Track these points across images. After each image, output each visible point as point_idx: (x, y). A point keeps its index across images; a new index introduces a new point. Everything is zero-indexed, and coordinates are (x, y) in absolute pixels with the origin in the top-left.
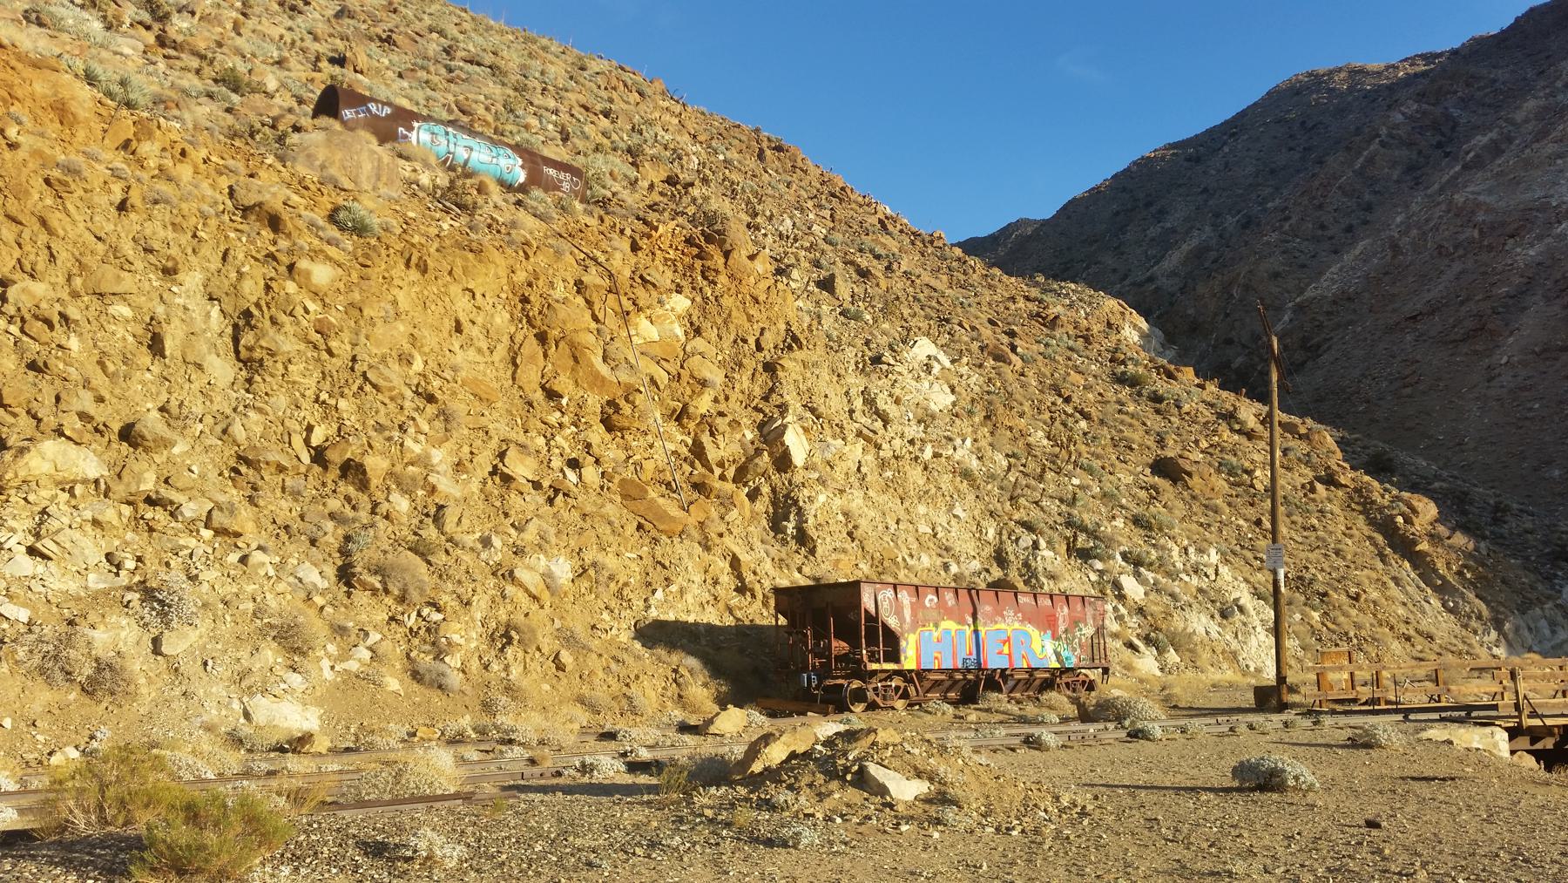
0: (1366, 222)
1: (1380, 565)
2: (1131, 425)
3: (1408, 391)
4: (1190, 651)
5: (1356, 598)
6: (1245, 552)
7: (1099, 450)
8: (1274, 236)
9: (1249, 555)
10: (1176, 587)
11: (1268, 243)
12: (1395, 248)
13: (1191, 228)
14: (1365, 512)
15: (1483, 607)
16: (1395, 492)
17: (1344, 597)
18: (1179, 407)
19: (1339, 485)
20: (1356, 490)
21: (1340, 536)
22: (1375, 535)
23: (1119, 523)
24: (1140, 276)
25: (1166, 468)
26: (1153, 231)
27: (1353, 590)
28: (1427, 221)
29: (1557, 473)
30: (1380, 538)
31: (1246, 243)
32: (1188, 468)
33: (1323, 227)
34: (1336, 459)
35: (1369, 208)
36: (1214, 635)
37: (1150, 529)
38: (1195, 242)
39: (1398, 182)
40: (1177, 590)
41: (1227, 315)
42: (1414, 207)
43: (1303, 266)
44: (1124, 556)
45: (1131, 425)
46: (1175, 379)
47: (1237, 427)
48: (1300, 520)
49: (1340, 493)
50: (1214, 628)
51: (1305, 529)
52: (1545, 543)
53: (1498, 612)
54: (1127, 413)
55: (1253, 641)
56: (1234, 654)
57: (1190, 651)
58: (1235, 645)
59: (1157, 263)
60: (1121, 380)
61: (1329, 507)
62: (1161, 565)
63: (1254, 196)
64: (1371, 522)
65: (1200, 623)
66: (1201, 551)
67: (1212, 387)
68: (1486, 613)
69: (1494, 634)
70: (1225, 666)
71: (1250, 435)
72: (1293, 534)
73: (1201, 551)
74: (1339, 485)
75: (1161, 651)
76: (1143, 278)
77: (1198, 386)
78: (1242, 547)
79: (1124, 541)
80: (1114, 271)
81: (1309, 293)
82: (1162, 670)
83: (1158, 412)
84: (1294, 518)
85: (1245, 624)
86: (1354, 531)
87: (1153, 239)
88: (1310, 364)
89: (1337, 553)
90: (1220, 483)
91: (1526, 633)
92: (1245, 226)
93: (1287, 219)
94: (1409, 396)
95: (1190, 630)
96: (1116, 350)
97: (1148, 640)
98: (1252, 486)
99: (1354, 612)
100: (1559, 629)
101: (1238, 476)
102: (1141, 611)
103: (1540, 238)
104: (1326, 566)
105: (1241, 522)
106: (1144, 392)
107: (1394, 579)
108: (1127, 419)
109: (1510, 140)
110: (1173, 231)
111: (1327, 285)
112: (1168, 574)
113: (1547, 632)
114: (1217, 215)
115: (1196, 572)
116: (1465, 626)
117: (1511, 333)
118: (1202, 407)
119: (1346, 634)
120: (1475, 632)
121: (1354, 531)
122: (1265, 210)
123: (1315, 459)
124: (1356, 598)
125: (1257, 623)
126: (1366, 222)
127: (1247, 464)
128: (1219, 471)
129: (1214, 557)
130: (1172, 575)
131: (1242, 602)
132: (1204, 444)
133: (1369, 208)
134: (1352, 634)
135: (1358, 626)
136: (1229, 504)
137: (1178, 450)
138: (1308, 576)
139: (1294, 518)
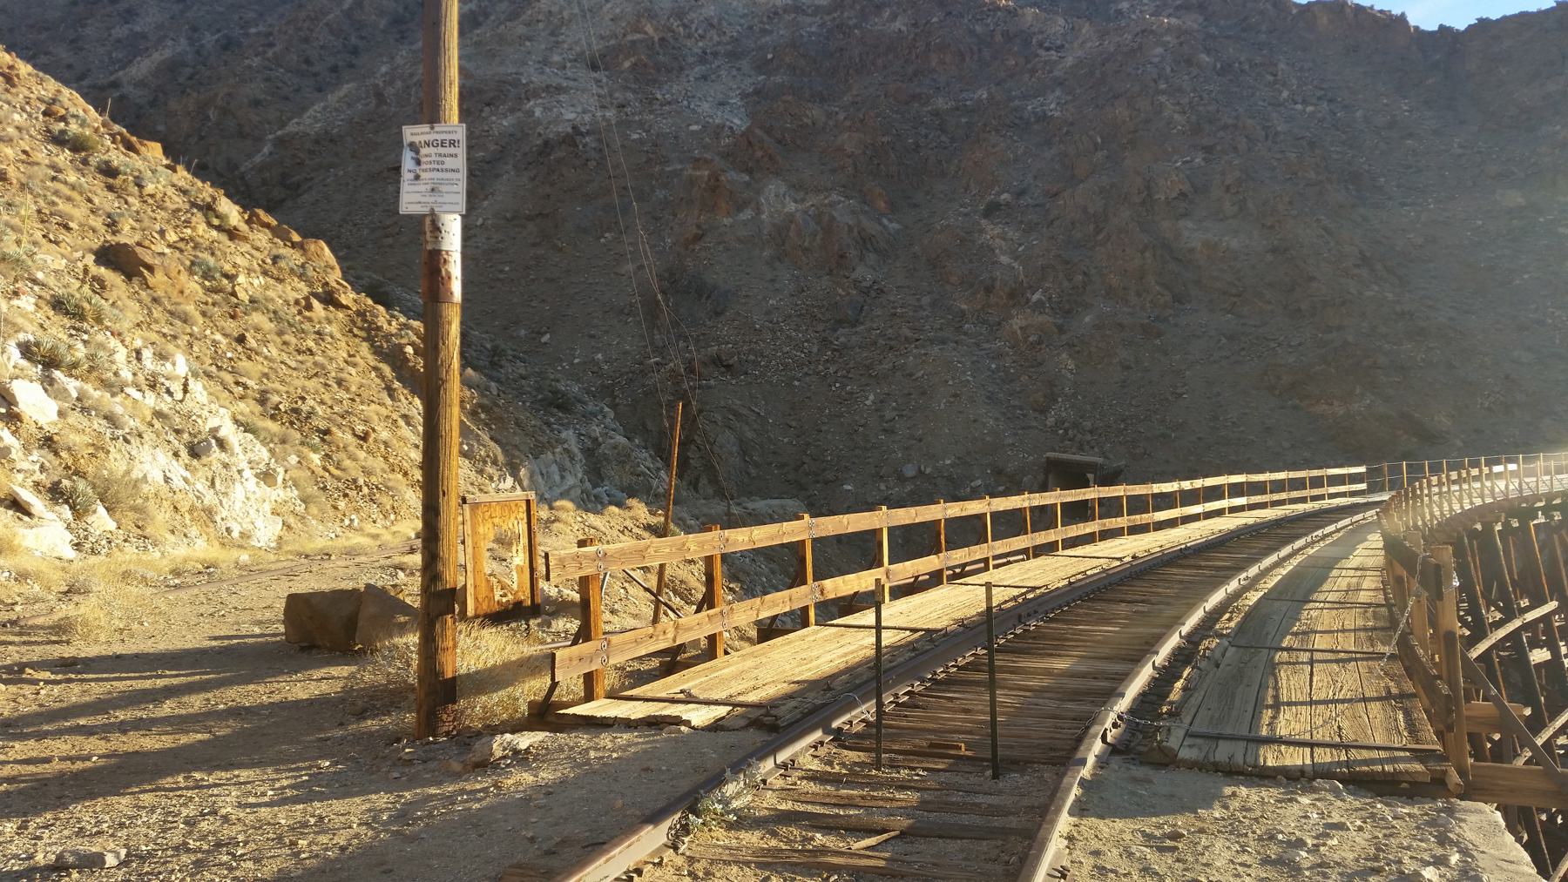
0: (351, 66)
1: (389, 402)
2: (69, 199)
3: (390, 241)
4: (134, 509)
5: (364, 438)
6: (223, 374)
7: (16, 221)
8: (256, 62)
9: (229, 378)
10: (117, 405)
11: (250, 67)
12: (380, 97)
13: (165, 37)
14: (369, 339)
15: (498, 450)
16: (403, 319)
17: (349, 437)
18: (140, 187)
19: (339, 306)
20: (359, 313)
21: (342, 365)
22: (381, 365)
23: (27, 303)
24: (103, 80)
25: (111, 256)
26: (120, 31)
27: (360, 428)
28: (411, 75)
29: (523, 332)
30: (387, 370)
31: (226, 63)
32: (148, 259)
33: (308, 61)
34: (335, 276)
35: (355, 51)
36: (178, 483)
37: (82, 318)
38: (168, 53)
39: (383, 31)
40: (119, 410)
41: (202, 138)
42: (399, 61)
43: (287, 98)
44: (27, 350)
45: (69, 199)
46: (137, 152)
47: (216, 222)
48: (293, 340)
49: (340, 315)
50: (177, 471)
51: (299, 352)
52: (539, 390)
53: (514, 457)
54: (66, 183)
55: (238, 492)
56: (209, 512)
57: (134, 509)
58: (210, 498)
59: (123, 68)
60: (59, 140)
61: (328, 329)
62: (93, 369)
63: (236, 17)
64: (377, 351)
65: (154, 464)
66: (162, 356)
67: (182, 172)
68: (501, 458)
69: (510, 481)
70: (194, 531)
71: (233, 234)
72: (285, 357)
73: (162, 356)
74: (339, 306)
75: (79, 512)
76: (105, 82)
77: (167, 167)
78: (219, 368)
79: (30, 328)
80: (70, 66)
81: (292, 127)
82: (78, 546)
83: (110, 188)
84: (286, 337)
85: (226, 466)
86: (358, 359)
87: (119, 41)
88: (289, 203)
89: (340, 382)
90: (193, 286)
91: (540, 479)
92: (226, 48)
93: (271, 45)
94: (391, 246)
95: (136, 474)
96: (54, 101)
97: (56, 493)
98: (234, 294)
99: (362, 455)
100: (567, 474)
101: (218, 284)
102: (48, 442)
103: (512, 111)
104: (326, 397)
105: (218, 337)
106: (93, 161)
107: (405, 417)
108: (65, 190)
109: (487, 15)
110: (144, 36)
111: (311, 120)
112: (105, 384)
113: (557, 478)
114: (195, 29)
115: (153, 387)
116: (481, 472)
117: (486, 198)
118: (170, 191)
119: (355, 481)
120: (491, 478)
121: (358, 359)
122: (247, 35)
123: (310, 273)
124: (364, 438)
125: (244, 465)
126: (351, 66)
127: (227, 267)
128: (191, 273)
129: (180, 365)
130: (114, 387)
131: (221, 434)
132: (172, 237)
133: (355, 51)
134: (361, 482)
135: (367, 472)
136: (204, 314)
137: (137, 238)
138: (305, 408)
139: (286, 337)
